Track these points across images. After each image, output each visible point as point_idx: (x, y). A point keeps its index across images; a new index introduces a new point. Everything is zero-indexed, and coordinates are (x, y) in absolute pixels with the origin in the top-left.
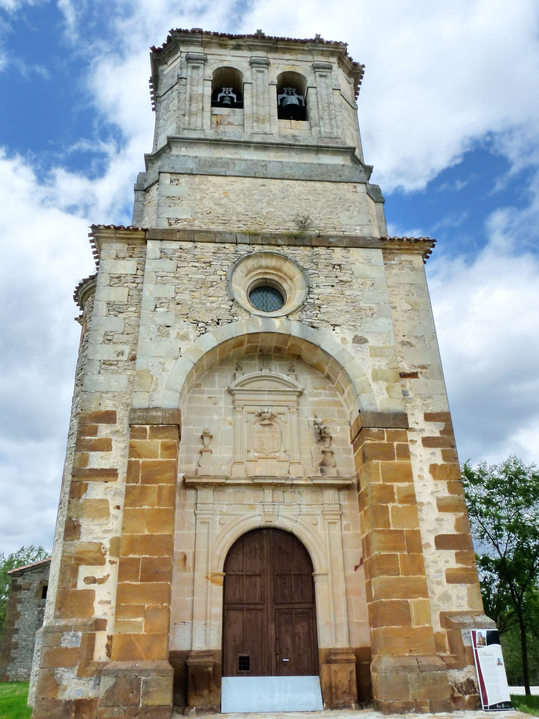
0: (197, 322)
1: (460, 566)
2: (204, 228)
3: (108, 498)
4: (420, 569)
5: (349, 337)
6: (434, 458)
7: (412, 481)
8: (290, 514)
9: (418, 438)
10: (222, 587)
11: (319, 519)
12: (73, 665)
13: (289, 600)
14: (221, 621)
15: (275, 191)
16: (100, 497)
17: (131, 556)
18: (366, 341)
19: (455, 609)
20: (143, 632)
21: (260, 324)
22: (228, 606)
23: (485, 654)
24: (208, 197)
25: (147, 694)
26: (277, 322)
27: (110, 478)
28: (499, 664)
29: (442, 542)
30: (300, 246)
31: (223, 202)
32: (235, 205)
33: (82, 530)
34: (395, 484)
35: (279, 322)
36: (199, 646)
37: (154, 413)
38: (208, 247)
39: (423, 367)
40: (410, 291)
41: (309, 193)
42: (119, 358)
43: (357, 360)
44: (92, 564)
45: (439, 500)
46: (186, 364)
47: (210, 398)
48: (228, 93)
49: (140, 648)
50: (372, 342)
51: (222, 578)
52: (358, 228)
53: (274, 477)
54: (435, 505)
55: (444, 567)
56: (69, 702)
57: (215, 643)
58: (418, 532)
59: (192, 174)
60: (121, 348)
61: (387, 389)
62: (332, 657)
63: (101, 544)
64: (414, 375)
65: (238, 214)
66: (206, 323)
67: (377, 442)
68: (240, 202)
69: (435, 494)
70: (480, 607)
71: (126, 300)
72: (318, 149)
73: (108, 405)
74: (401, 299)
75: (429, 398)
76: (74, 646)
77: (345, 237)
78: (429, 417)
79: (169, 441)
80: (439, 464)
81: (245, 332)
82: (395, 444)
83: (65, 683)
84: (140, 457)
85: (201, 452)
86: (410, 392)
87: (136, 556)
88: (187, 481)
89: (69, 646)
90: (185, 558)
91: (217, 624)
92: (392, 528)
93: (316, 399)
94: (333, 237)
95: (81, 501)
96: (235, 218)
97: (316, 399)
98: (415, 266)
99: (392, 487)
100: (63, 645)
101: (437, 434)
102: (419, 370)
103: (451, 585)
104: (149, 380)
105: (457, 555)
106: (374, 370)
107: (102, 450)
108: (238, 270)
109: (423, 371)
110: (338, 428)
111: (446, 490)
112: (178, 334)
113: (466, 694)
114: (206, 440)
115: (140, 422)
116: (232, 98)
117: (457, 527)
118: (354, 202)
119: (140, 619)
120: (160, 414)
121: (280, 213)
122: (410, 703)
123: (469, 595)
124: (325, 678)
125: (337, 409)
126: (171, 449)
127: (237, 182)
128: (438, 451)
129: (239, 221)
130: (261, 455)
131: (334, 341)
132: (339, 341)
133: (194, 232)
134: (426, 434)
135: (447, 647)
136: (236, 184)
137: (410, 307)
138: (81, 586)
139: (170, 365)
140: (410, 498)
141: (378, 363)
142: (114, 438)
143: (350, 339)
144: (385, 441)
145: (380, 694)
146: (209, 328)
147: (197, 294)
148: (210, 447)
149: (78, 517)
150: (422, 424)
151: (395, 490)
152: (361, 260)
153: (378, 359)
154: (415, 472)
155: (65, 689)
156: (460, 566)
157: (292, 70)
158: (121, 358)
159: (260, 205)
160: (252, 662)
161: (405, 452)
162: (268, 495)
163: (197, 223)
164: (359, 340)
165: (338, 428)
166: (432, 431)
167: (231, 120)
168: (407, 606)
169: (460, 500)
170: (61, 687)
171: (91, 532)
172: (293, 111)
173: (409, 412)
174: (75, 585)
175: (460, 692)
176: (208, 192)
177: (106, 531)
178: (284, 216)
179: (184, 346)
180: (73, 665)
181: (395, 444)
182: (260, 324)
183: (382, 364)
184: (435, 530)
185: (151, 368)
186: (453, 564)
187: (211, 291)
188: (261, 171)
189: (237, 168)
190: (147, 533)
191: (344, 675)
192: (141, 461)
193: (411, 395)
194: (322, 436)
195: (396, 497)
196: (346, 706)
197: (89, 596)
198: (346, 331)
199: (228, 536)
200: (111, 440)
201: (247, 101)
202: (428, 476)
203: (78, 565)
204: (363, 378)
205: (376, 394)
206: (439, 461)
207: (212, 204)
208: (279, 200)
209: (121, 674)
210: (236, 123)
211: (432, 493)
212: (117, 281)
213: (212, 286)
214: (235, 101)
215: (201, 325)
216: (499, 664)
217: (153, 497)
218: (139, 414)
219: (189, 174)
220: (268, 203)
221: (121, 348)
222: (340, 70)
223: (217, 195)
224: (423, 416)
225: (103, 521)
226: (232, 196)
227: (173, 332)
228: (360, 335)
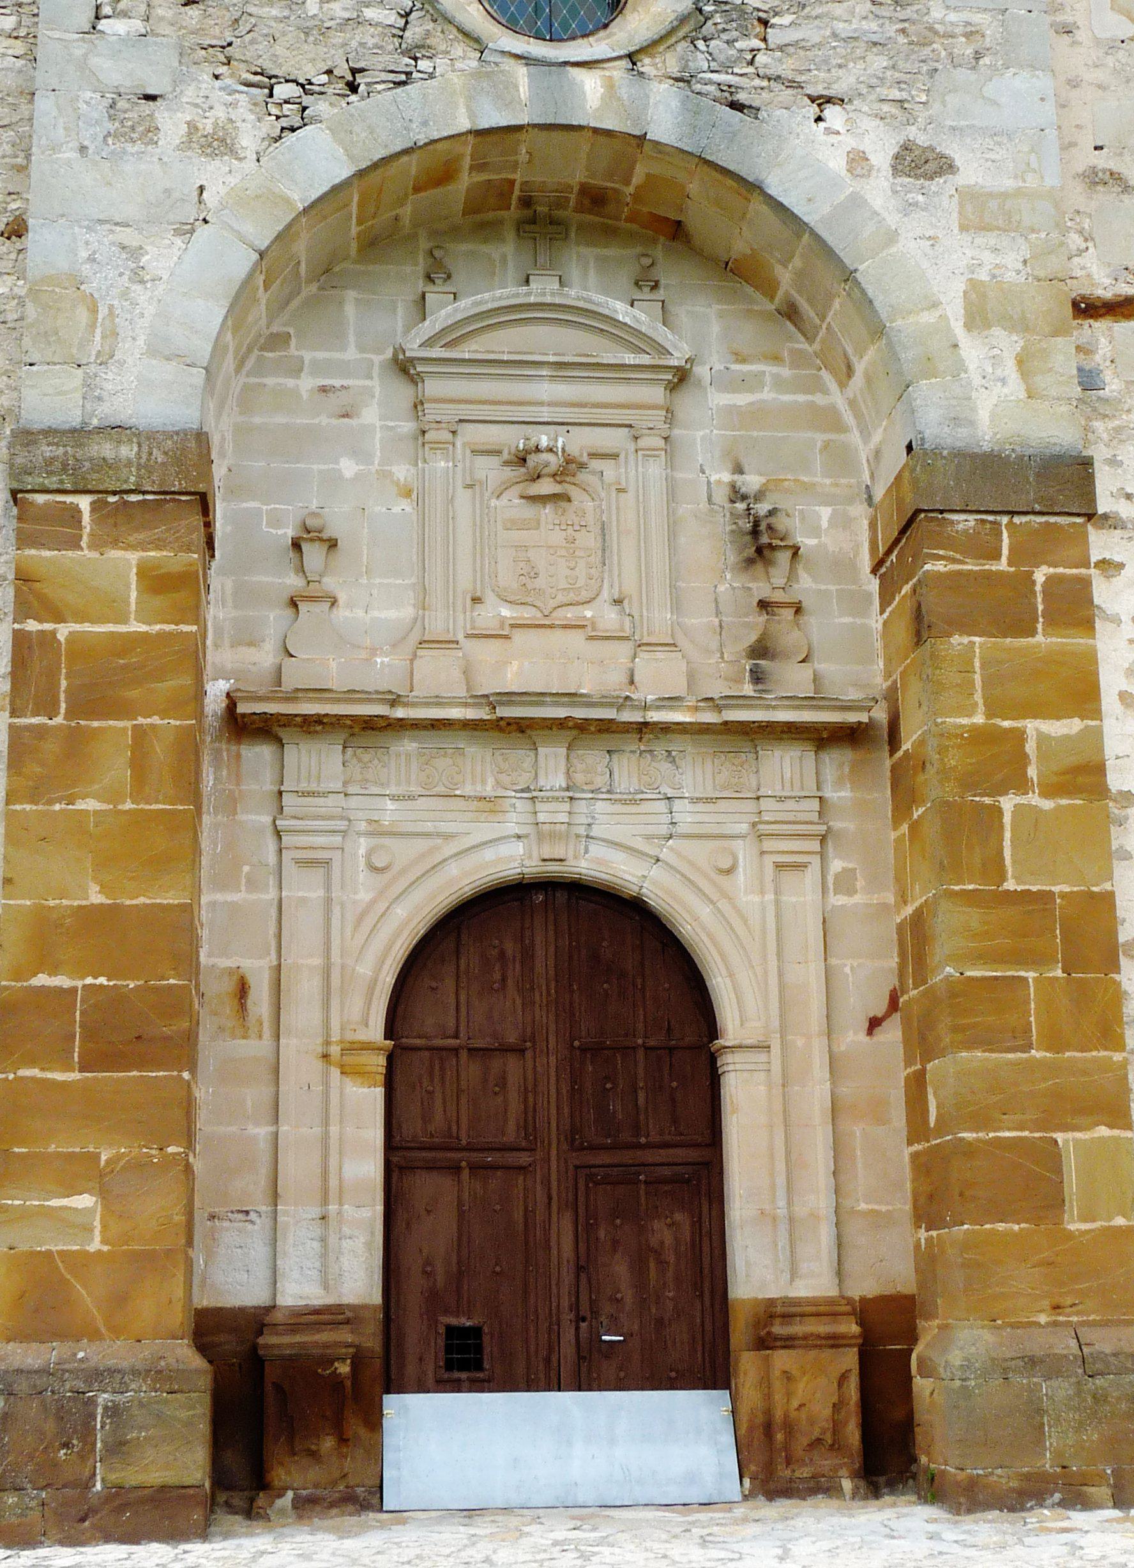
0: (266, 81)
5: (881, 149)
8: (628, 835)
11: (744, 851)
14: (380, 1208)
17: (42, 980)
18: (946, 167)
20: (95, 1245)
21: (524, 91)
26: (590, 84)
34: (1032, 726)
36: (300, 1290)
43: (909, 246)
46: (226, 255)
47: (324, 389)
49: (88, 1298)
50: (971, 172)
51: (382, 1061)
53: (572, 698)
57: (358, 1280)
58: (1108, 898)
61: (1021, 362)
62: (774, 1326)
81: (463, 124)
82: (1040, 575)
84: (60, 619)
85: (293, 604)
86: (1108, 376)
87: (62, 981)
88: (242, 708)
90: (242, 990)
92: (1010, 885)
93: (742, 399)
97: (742, 399)
99: (1019, 736)
104: (82, 315)
106: (973, 284)
112: (192, 127)
114: (313, 554)
115: (52, 482)
119: (85, 1201)
120: (127, 451)
124: (750, 1394)
125: (820, 438)
126: (181, 590)
131: (818, 163)
132: (837, 163)
139: (163, 256)
143: (881, 157)
146: (319, 107)
148: (330, 583)
151: (1030, 747)
153: (992, 239)
162: (551, 764)
168: (1052, 1156)
179: (219, 178)
181: (1040, 575)
182: (524, 91)
183: (1006, 261)
185: (86, 269)
190: (96, 897)
191: (818, 1389)
192: (63, 632)
194: (761, 542)
195: (1032, 772)
196: (819, 1487)
199: (400, 912)
204: (928, 318)
215: (283, 91)
217: (117, 769)
218: (47, 451)
227: (171, 123)
228: (922, 140)
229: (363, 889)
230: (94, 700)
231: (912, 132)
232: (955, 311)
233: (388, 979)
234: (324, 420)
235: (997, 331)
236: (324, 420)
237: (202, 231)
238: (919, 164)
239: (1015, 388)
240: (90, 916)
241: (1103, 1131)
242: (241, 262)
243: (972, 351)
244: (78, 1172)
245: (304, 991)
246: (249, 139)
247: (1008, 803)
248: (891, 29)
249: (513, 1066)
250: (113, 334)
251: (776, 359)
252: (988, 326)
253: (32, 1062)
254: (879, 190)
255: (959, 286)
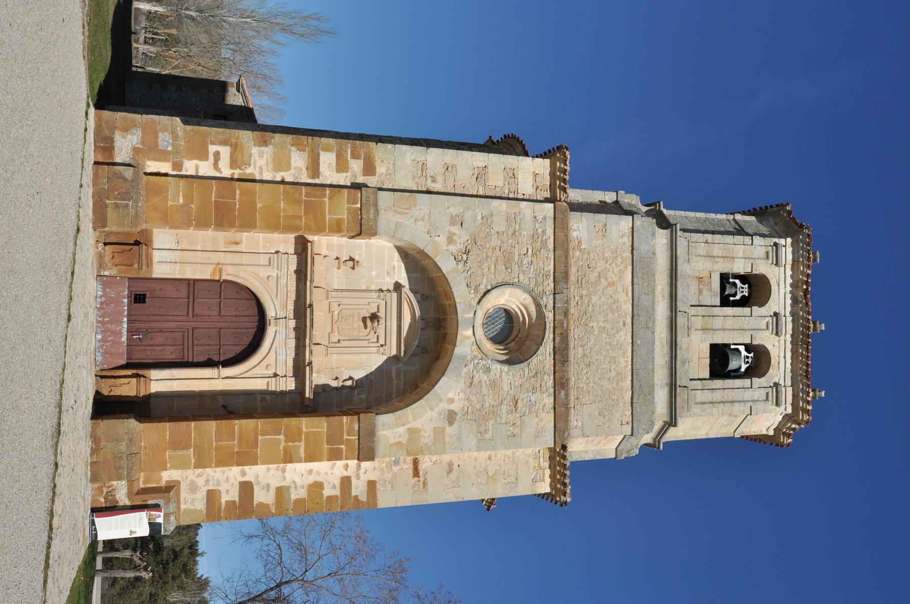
0: (467, 252)
1: (223, 504)
2: (572, 261)
3: (292, 171)
4: (221, 463)
5: (456, 406)
6: (330, 486)
7: (306, 461)
9: (350, 472)
10: (209, 277)
12: (143, 145)
13: (195, 342)
14: (178, 277)
15: (618, 336)
16: (293, 164)
17: (238, 192)
18: (451, 423)
19: (182, 496)
20: (170, 203)
21: (467, 316)
22: (191, 284)
23: (140, 519)
24: (608, 267)
25: (117, 206)
26: (469, 332)
27: (311, 172)
28: (131, 532)
29: (246, 488)
30: (554, 359)
31: (602, 280)
32: (600, 293)
33: (262, 148)
34: (303, 444)
35: (470, 338)
36: (157, 256)
37: (372, 211)
38: (549, 264)
39: (425, 484)
40: (509, 476)
41: (618, 373)
42: (429, 178)
43: (430, 414)
44: (231, 158)
45: (288, 488)
46: (422, 243)
47: (394, 268)
48: (742, 290)
49: (156, 201)
50: (449, 430)
51: (217, 278)
52: (580, 424)
53: (312, 326)
54: (282, 484)
55: (222, 488)
56: (112, 140)
57: (160, 270)
58: (256, 464)
59: (633, 250)
60: (440, 179)
61: (400, 442)
63: (250, 165)
64: (416, 473)
65: (589, 295)
66: (466, 262)
67: (345, 428)
68: (603, 299)
69: (293, 486)
70: (184, 522)
71: (490, 183)
72: (673, 386)
73: (381, 169)
74: (500, 465)
75: (392, 487)
76: (160, 142)
77: (567, 409)
78: (372, 485)
79: (345, 224)
80: (324, 492)
81: (457, 300)
82: (343, 446)
83: (129, 137)
84: (329, 199)
85: (337, 258)
86: (398, 467)
87: (238, 197)
88: (309, 244)
89: (160, 139)
90: (237, 243)
91: (175, 272)
92: (260, 437)
93: (394, 375)
94: (567, 395)
95: (289, 147)
96: (584, 292)
97: (394, 375)
98: (538, 484)
99: (300, 441)
100: (160, 134)
101: (354, 493)
102: (422, 479)
103: (205, 493)
104: (406, 207)
105: (234, 502)
106: (420, 430)
107: (337, 164)
108: (526, 295)
109: (421, 483)
110: (364, 397)
111: (298, 497)
112: (454, 234)
113: (105, 498)
114: (351, 264)
115: (364, 198)
116: (735, 295)
117: (261, 504)
118: (609, 420)
119: (181, 200)
120: (372, 216)
121: (592, 340)
122: (100, 442)
123: (195, 511)
125: (384, 396)
126: (337, 228)
127: (627, 296)
128: (337, 492)
129: (581, 297)
130: (336, 318)
132: (451, 395)
133: (566, 251)
134: (354, 480)
135: (148, 486)
136: (624, 295)
137: (491, 475)
138: (212, 149)
139: (422, 227)
140: (289, 458)
141: (426, 435)
142: (349, 174)
143: (452, 407)
144: (345, 437)
145: (106, 425)
146: (461, 265)
147: (497, 253)
148: (343, 267)
149: (274, 144)
150: (365, 478)
151: (297, 443)
152: (541, 425)
153: (432, 435)
154: (315, 466)
155: (123, 137)
156: (223, 504)
157: (773, 361)
158: (429, 179)
159: (602, 318)
160: (140, 305)
161: (335, 456)
163: (578, 253)
164: (451, 417)
165: (364, 397)
166: (357, 487)
167: (705, 292)
168: (186, 447)
169: (287, 510)
170: (125, 134)
171: (261, 156)
172: (720, 361)
173: (376, 463)
174: (213, 143)
175: (107, 493)
176: (613, 265)
177: (261, 168)
178: (590, 344)
179: (442, 240)
180: (143, 143)
181: (343, 446)
182: (467, 316)
183: (427, 438)
184: (258, 483)
185: (418, 207)
186: (224, 499)
187: (501, 267)
188: (641, 321)
189: (643, 297)
190: (259, 205)
192: (326, 199)
193: (395, 469)
195: (290, 444)
197: (204, 156)
198: (462, 403)
199: (257, 284)
200: (347, 172)
201: (729, 310)
202: (312, 479)
203: (231, 146)
204: (411, 418)
205: (395, 430)
206: (327, 492)
207: (599, 269)
208: (608, 340)
209: (134, 184)
210: (701, 298)
211: (294, 482)
212: (510, 174)
213: (506, 268)
214: (731, 299)
215: (465, 257)
216: (131, 532)
217: (291, 212)
218: (371, 197)
219: (632, 246)
220: (604, 328)
221: (440, 179)
222: (780, 418)
223: (610, 274)
224: (374, 479)
225: (271, 166)
226: (610, 290)
227: (455, 229)
228: (458, 418)
229: (263, 272)
230: (309, 207)
231: (460, 415)
232: (413, 425)
233: (239, 281)
234: (386, 268)
235: (407, 437)
236: (386, 268)
237: (428, 236)
238: (451, 417)
239: (392, 441)
240: (255, 204)
241: (193, 461)
242: (421, 245)
243: (402, 430)
244: (189, 199)
245: (237, 258)
246: (452, 248)
247: (282, 437)
248: (487, 410)
249: (216, 313)
250: (401, 213)
251: (405, 384)
252: (409, 434)
253: (217, 189)
254: (444, 406)
255: (420, 427)
